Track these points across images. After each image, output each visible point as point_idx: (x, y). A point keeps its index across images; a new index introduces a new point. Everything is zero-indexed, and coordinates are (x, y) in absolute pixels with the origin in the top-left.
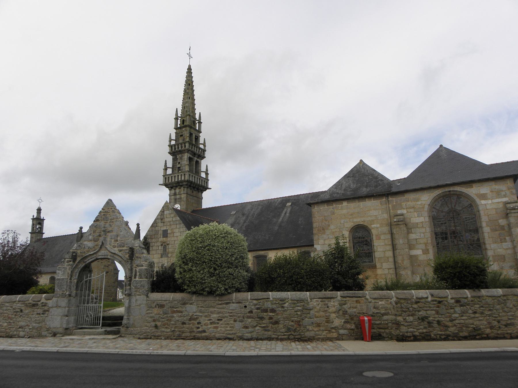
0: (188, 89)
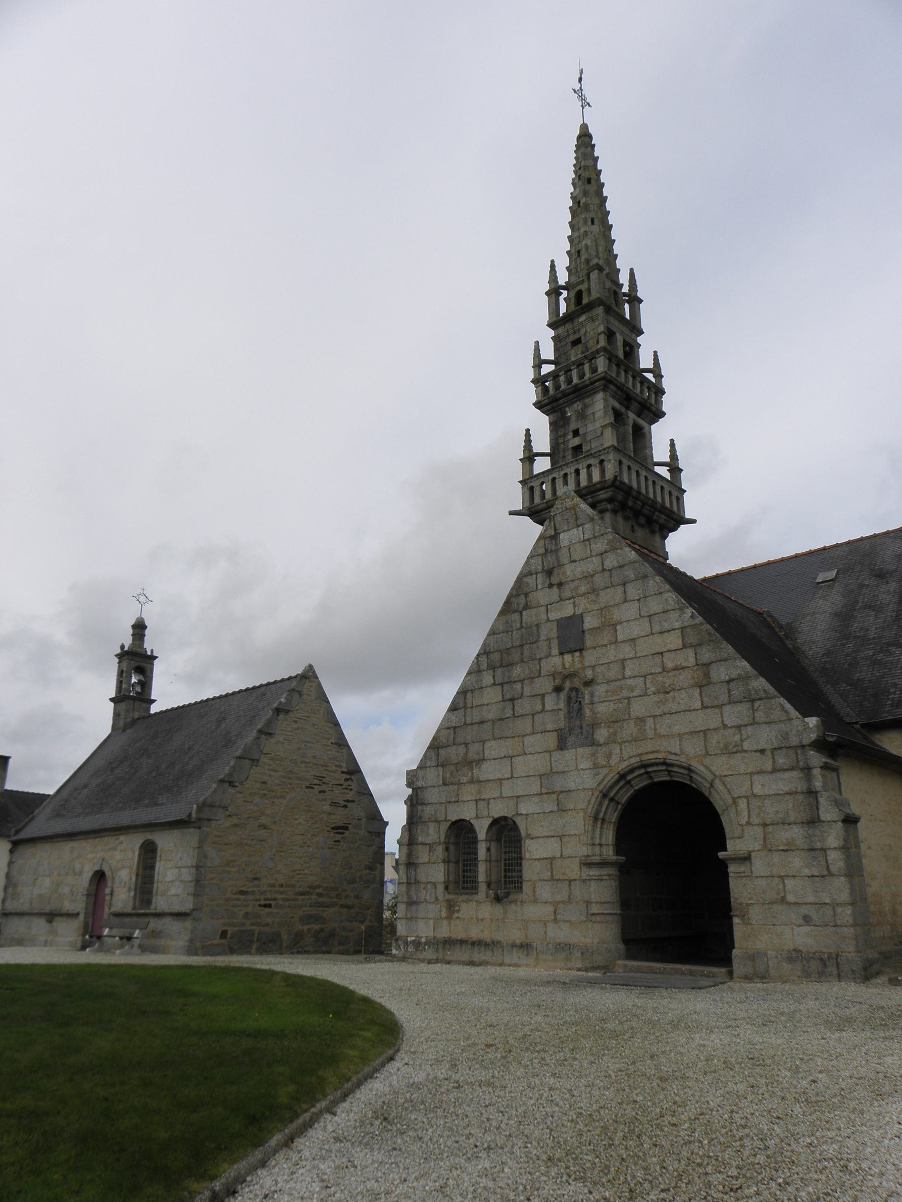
0: (585, 193)
